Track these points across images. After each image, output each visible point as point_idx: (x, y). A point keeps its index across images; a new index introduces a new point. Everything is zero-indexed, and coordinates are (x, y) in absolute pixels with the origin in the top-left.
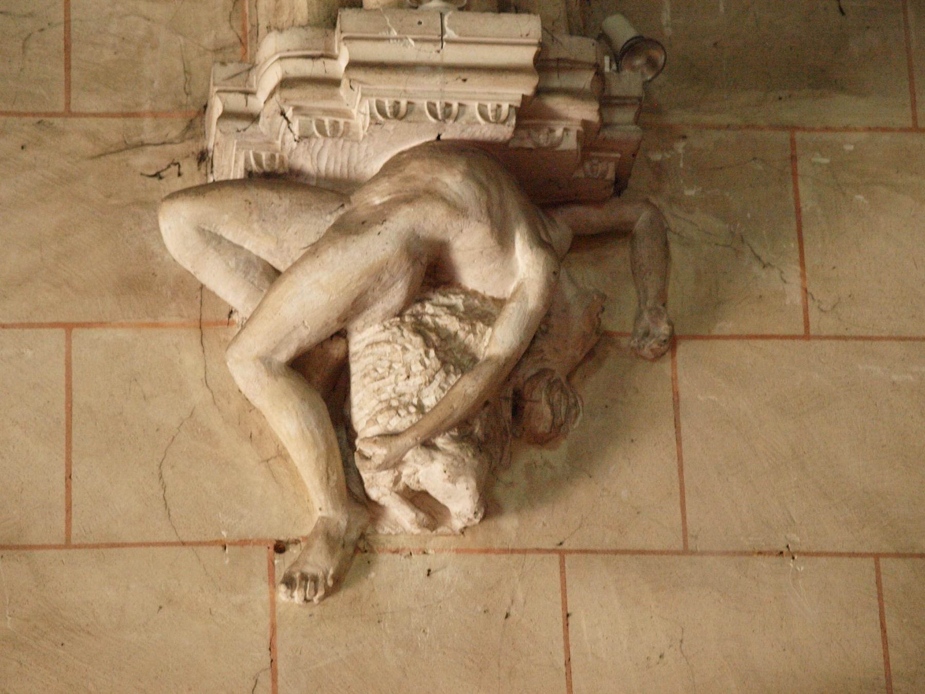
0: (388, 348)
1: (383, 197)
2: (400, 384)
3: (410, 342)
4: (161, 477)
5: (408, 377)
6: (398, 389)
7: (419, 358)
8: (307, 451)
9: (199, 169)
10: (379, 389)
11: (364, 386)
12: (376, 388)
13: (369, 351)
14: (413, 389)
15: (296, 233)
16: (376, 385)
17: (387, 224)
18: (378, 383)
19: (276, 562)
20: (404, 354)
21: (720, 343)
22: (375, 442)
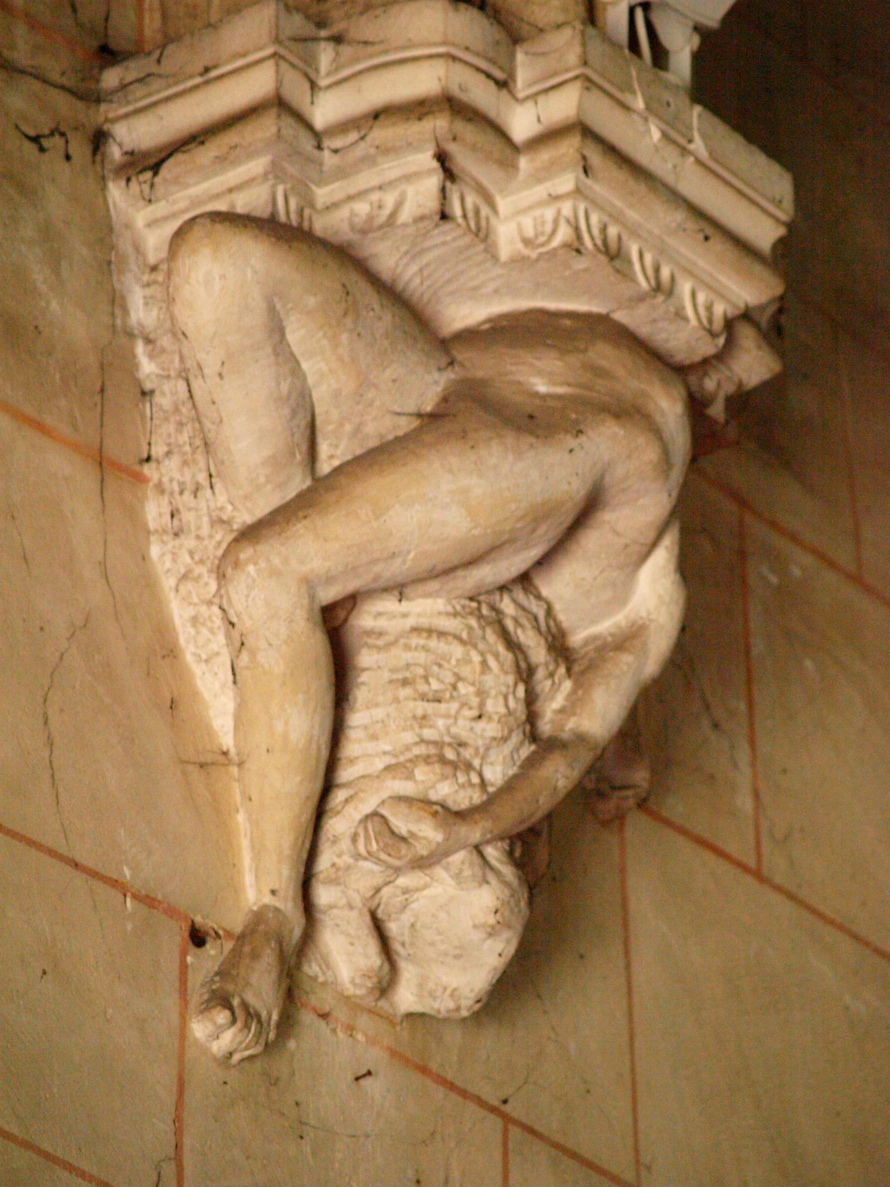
0: (457, 651)
1: (555, 384)
2: (461, 722)
3: (497, 656)
4: (46, 723)
5: (480, 717)
6: (454, 730)
7: (504, 689)
8: (298, 779)
9: (94, 162)
10: (424, 717)
11: (396, 700)
12: (419, 712)
13: (415, 641)
14: (480, 742)
15: (394, 381)
16: (421, 707)
17: (583, 439)
18: (425, 704)
19: (189, 959)
20: (483, 673)
21: (669, 833)
22: (435, 814)
